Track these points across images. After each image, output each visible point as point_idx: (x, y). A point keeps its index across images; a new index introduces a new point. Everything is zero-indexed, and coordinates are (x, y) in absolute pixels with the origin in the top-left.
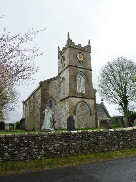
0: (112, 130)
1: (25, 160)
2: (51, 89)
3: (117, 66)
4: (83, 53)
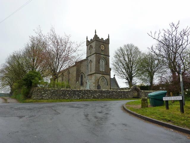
0: (119, 90)
1: (87, 99)
2: (82, 67)
3: (127, 50)
4: (104, 44)
